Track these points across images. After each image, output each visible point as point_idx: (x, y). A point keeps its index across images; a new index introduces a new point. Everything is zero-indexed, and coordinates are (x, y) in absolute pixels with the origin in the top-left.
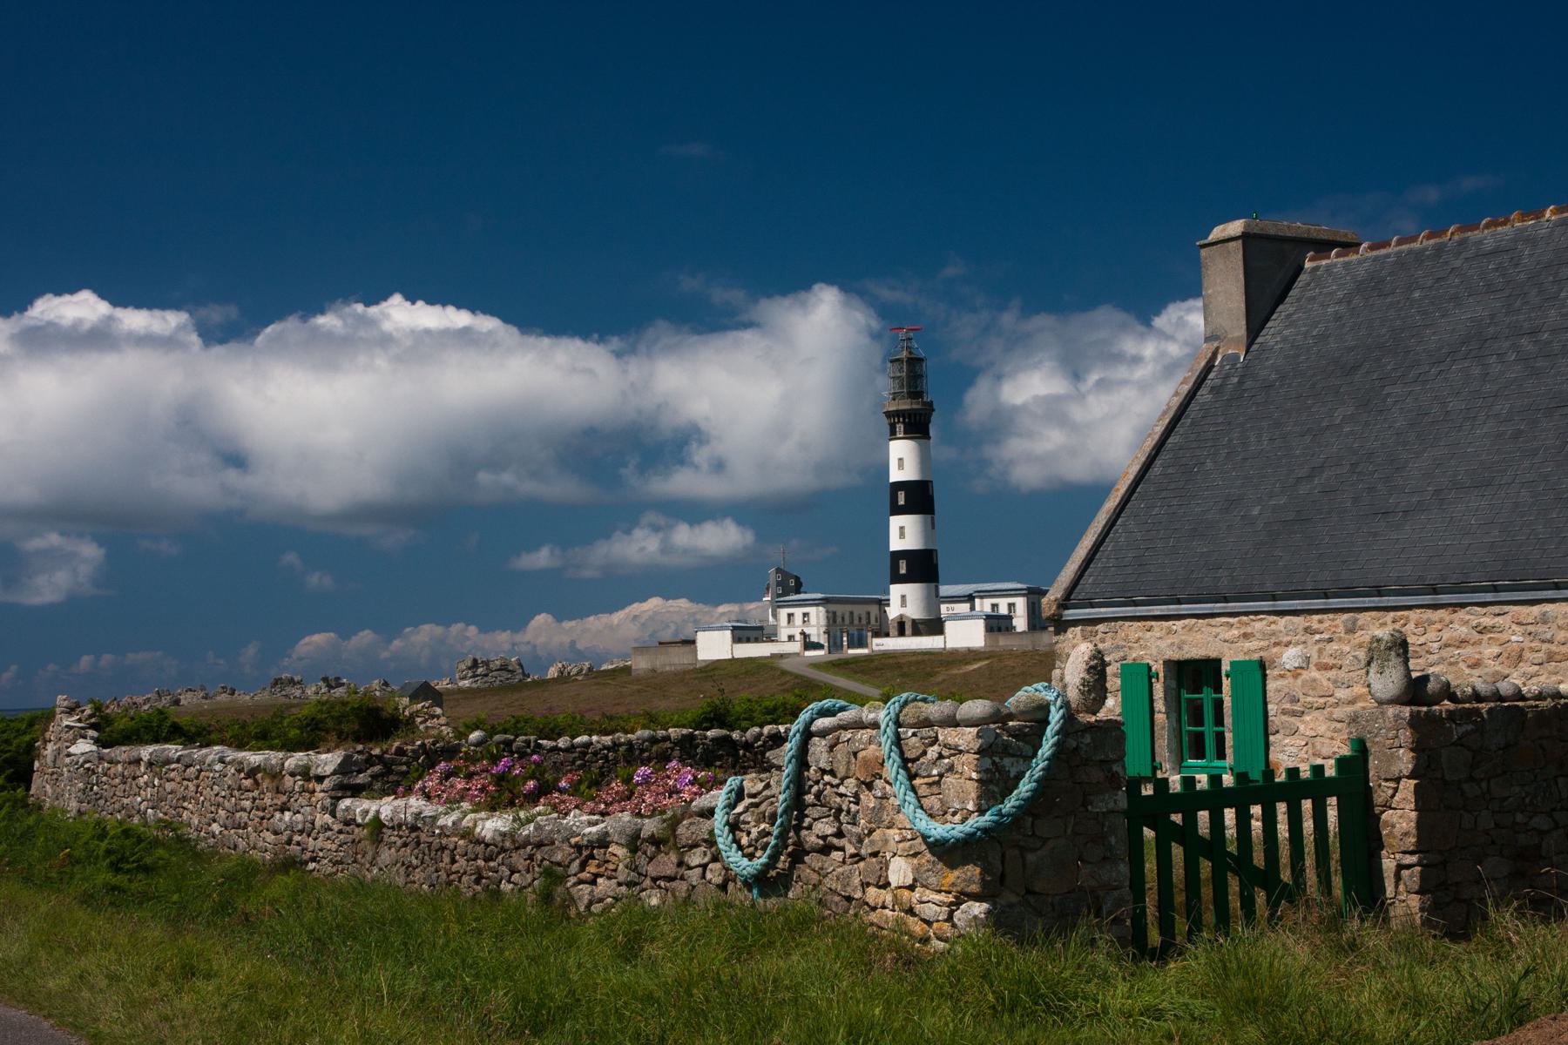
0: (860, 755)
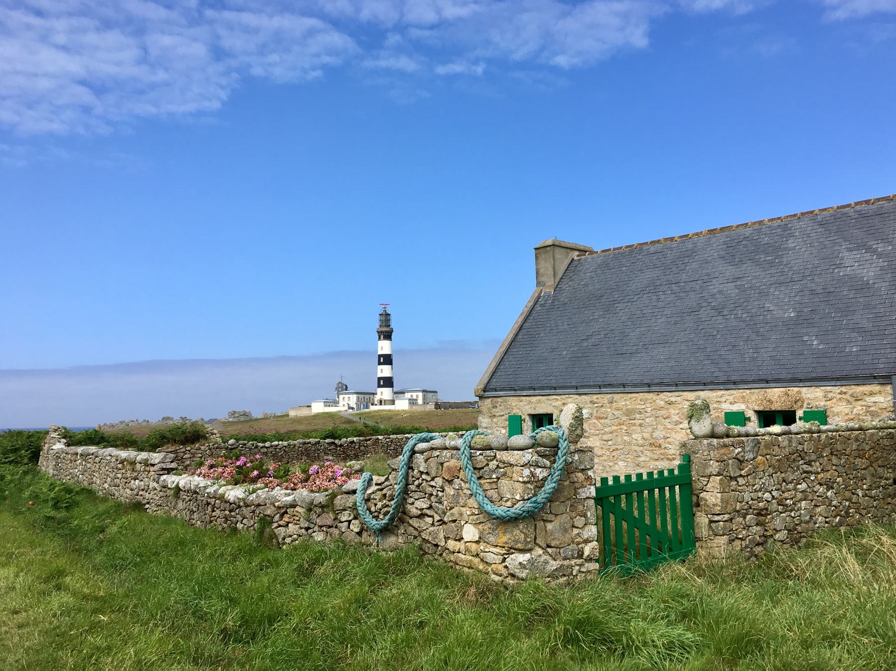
0: (445, 465)
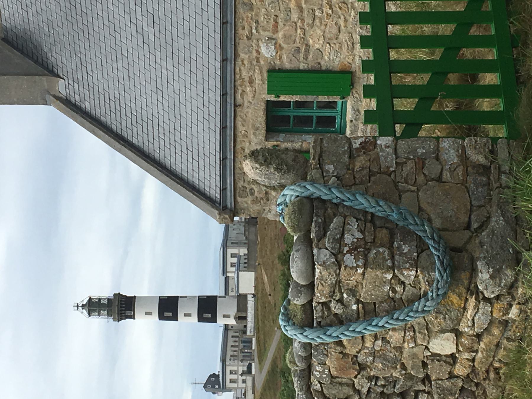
0: (334, 373)
